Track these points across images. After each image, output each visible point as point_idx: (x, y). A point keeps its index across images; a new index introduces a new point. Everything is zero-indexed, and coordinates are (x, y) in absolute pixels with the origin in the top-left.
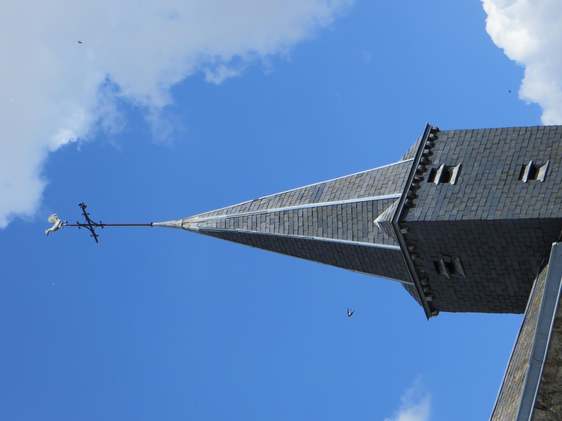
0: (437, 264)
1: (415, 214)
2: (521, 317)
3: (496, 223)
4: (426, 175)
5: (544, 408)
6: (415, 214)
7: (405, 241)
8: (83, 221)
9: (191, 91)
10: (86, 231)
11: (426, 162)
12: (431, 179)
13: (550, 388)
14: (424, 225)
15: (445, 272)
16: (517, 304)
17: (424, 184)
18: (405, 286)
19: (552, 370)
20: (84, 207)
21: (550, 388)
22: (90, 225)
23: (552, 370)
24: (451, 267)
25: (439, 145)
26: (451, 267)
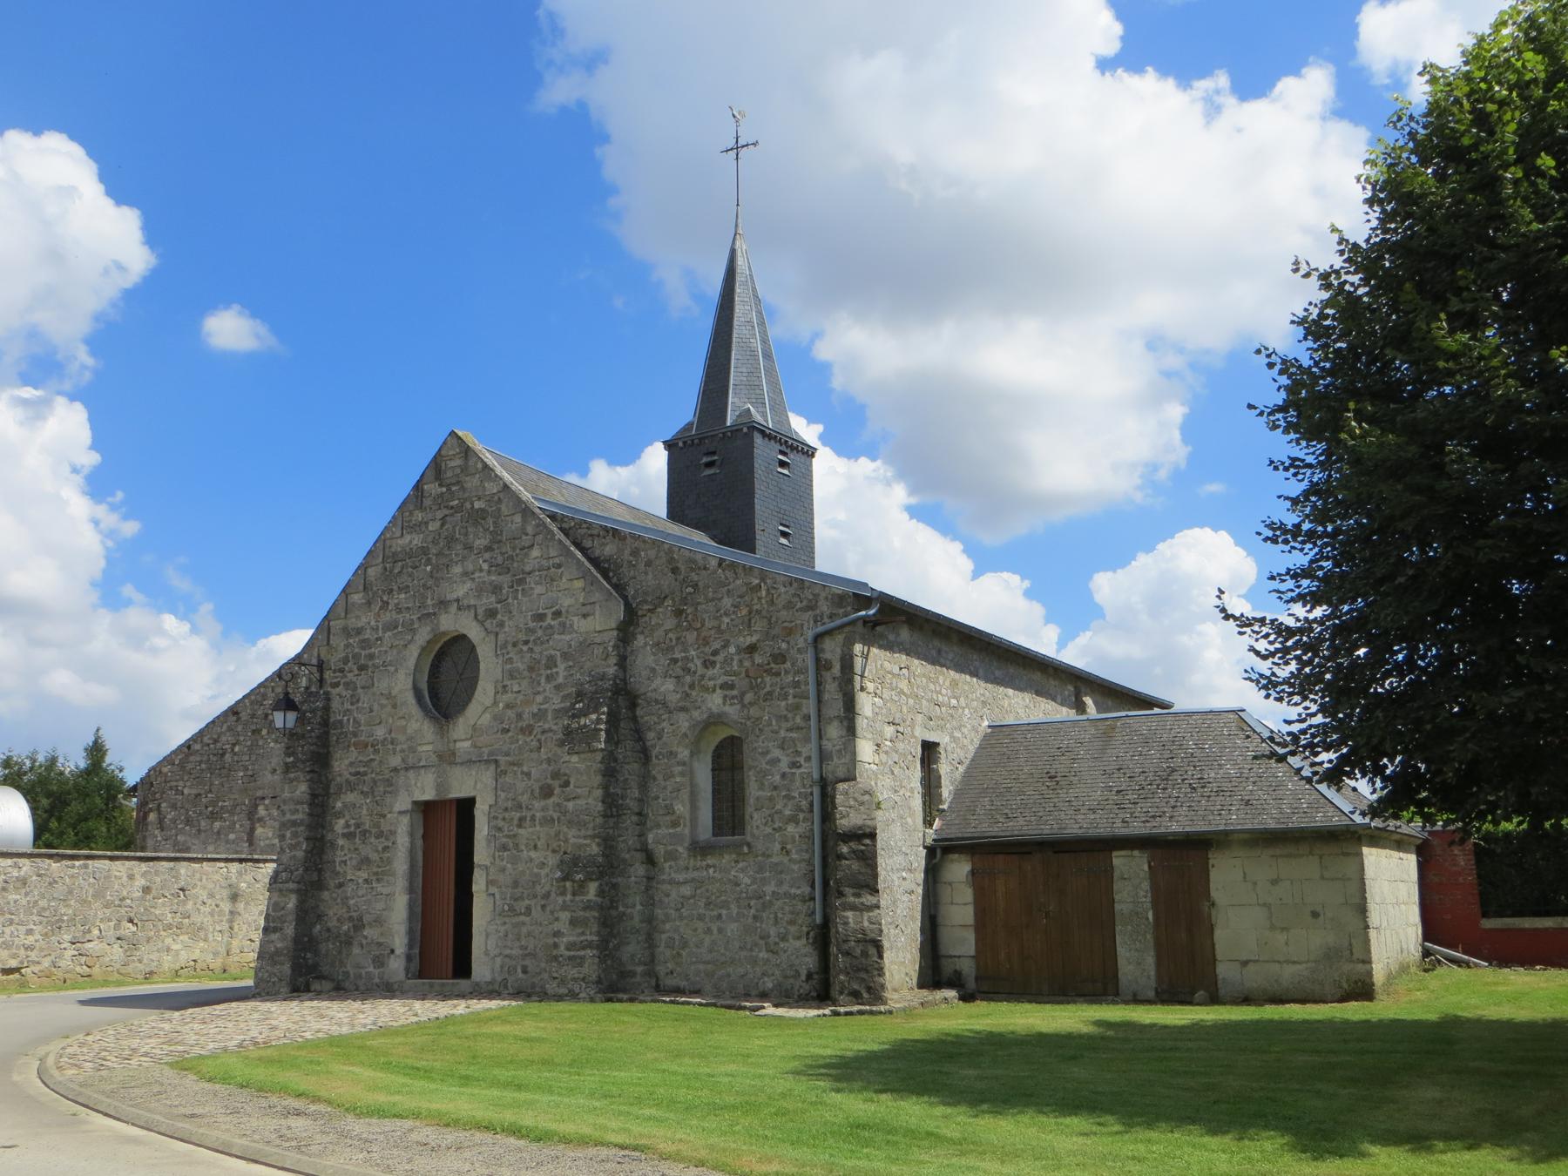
0: (714, 453)
1: (758, 439)
2: (664, 515)
3: (751, 506)
4: (783, 448)
5: (720, 565)
6: (758, 439)
7: (736, 431)
8: (741, 142)
9: (582, 132)
10: (732, 143)
11: (793, 448)
12: (782, 452)
13: (740, 571)
14: (751, 445)
15: (705, 460)
16: (677, 511)
17: (778, 447)
18: (690, 425)
19: (756, 573)
20: (1250, 407)
21: (740, 571)
22: (737, 148)
23: (756, 573)
24: (710, 465)
25: (804, 458)
26: (710, 465)
